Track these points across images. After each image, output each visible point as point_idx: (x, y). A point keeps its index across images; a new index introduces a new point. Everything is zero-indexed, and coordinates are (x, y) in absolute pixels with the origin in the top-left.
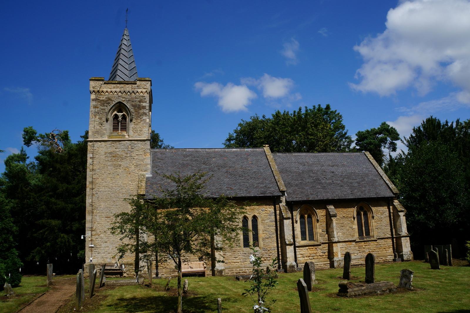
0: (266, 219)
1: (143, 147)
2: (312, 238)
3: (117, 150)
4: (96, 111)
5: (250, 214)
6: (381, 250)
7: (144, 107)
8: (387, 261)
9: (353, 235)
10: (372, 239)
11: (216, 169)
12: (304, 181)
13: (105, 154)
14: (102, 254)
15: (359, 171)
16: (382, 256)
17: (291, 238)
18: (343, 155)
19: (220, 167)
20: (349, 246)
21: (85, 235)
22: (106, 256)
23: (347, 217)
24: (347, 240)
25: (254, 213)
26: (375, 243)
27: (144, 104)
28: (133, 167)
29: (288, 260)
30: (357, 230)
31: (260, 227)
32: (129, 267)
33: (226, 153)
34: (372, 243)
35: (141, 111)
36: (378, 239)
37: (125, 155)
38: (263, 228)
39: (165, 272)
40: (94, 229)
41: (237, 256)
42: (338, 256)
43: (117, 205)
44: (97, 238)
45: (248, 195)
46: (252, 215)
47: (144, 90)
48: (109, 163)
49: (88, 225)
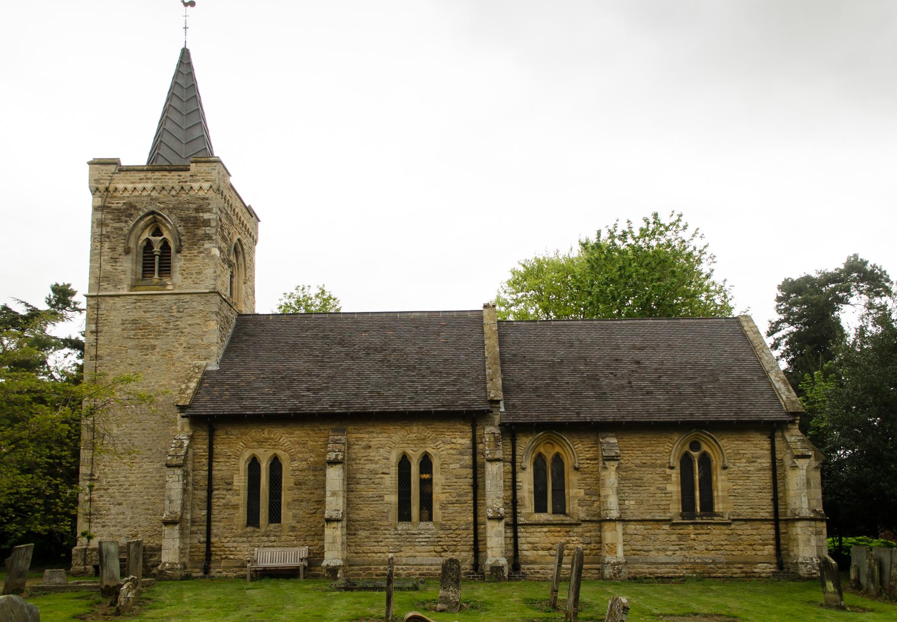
1: (201, 307)
2: (560, 507)
3: (148, 315)
4: (104, 233)
6: (740, 547)
7: (207, 223)
8: (757, 575)
9: (666, 507)
10: (717, 519)
11: (362, 354)
12: (557, 380)
13: (123, 324)
14: (112, 528)
15: (708, 361)
16: (740, 563)
17: (501, 505)
18: (679, 323)
19: (369, 350)
20: (650, 531)
22: (119, 533)
23: (653, 466)
24: (648, 517)
27: (206, 216)
28: (181, 349)
29: (489, 552)
33: (396, 321)
34: (716, 531)
35: (200, 232)
36: (734, 520)
37: (164, 325)
38: (443, 481)
39: (224, 567)
40: (95, 478)
42: (616, 553)
43: (144, 429)
44: (102, 496)
45: (413, 408)
46: (421, 451)
47: (206, 185)
48: (131, 343)
49: (84, 470)
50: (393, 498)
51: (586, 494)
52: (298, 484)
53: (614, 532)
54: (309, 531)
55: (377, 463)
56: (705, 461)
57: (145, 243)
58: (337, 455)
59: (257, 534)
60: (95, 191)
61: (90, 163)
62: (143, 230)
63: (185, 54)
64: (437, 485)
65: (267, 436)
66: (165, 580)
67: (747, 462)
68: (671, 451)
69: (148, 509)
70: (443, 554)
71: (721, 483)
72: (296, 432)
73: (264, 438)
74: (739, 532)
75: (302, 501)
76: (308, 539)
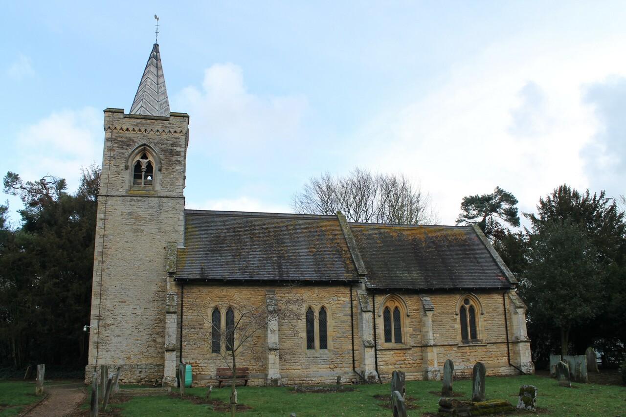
2: (399, 339)
6: (491, 359)
7: (178, 153)
9: (455, 337)
20: (448, 352)
23: (448, 313)
24: (446, 343)
27: (178, 149)
30: (459, 331)
31: (330, 322)
34: (480, 349)
35: (174, 158)
42: (433, 365)
43: (135, 286)
49: (94, 312)
51: (414, 331)
53: (432, 353)
56: (472, 310)
57: (136, 164)
59: (219, 358)
61: (105, 111)
62: (137, 155)
63: (156, 46)
64: (96, 260)
65: (225, 294)
66: (244, 408)
67: (493, 310)
68: (456, 305)
69: (137, 340)
70: (334, 369)
71: (481, 323)
72: (244, 292)
73: (224, 295)
74: (491, 350)
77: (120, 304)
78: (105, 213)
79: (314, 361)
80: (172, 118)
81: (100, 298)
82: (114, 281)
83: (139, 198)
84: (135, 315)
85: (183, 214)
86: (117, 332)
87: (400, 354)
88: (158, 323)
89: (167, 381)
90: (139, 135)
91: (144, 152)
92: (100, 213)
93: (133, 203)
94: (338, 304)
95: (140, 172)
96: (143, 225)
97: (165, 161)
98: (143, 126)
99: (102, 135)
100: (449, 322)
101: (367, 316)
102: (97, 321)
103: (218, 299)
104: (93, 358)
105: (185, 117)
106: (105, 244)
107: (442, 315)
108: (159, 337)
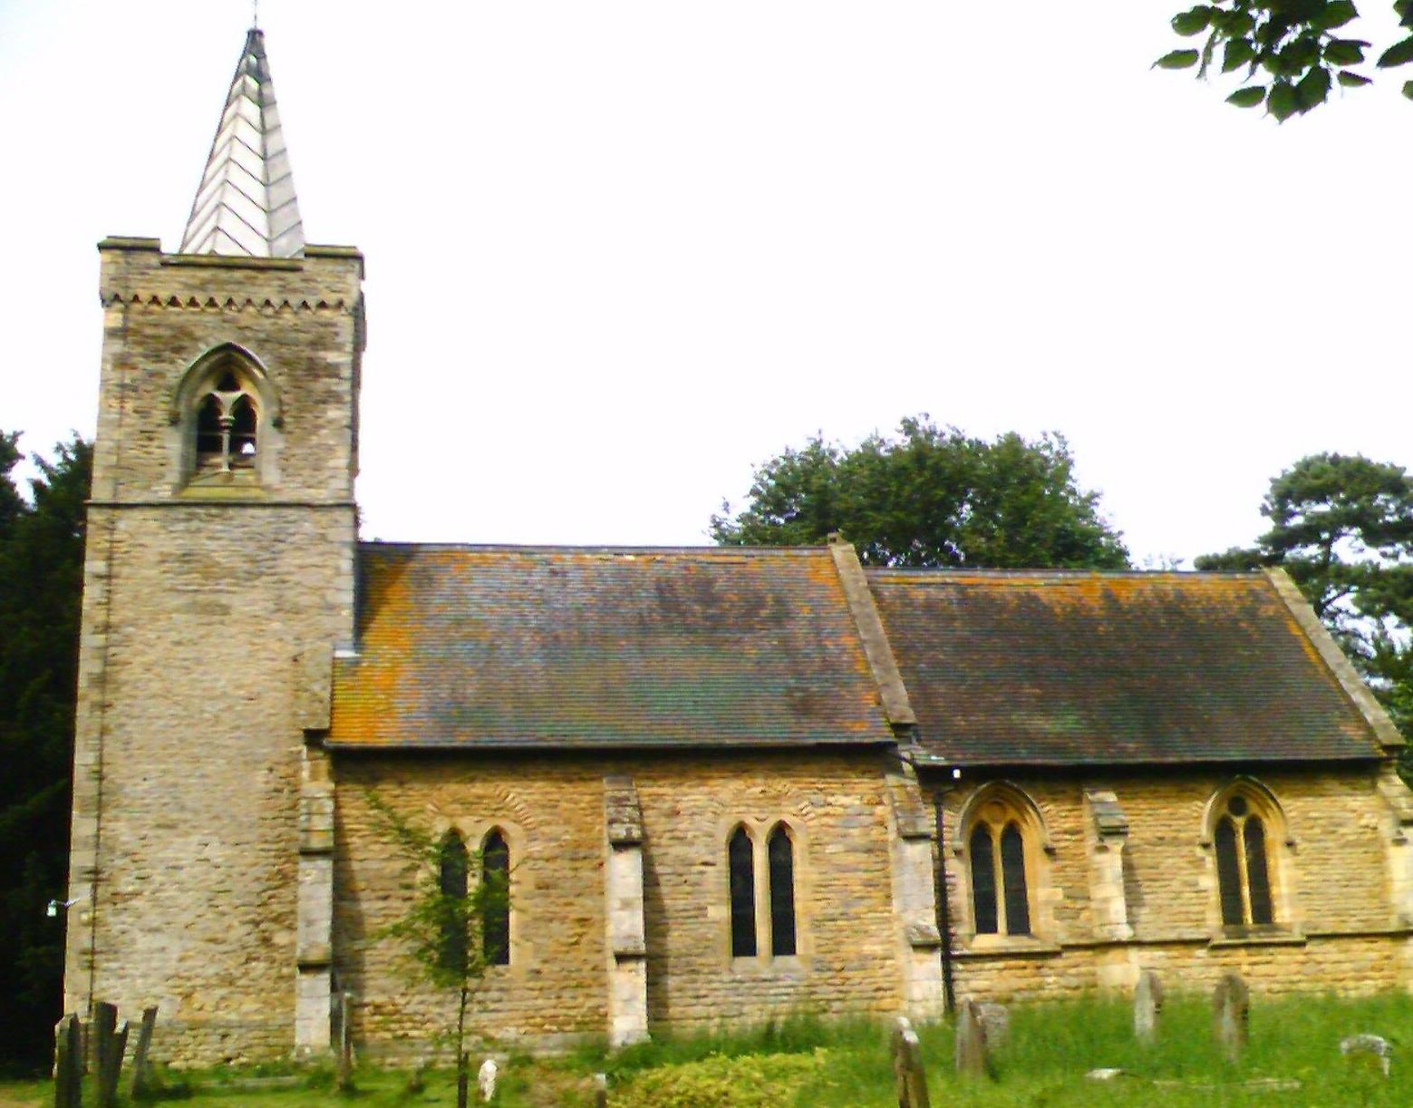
0: (826, 839)
2: (1019, 924)
4: (127, 381)
5: (763, 816)
7: (333, 371)
9: (1200, 917)
20: (1179, 962)
21: (66, 901)
23: (1175, 842)
24: (1172, 936)
25: (781, 812)
26: (1298, 955)
27: (332, 357)
30: (1214, 897)
31: (802, 872)
32: (250, 1035)
34: (1282, 956)
36: (1311, 937)
41: (703, 992)
49: (80, 859)
50: (721, 912)
52: (544, 886)
53: (1126, 965)
54: (565, 978)
55: (691, 844)
58: (629, 830)
60: (109, 300)
63: (255, 36)
67: (1324, 833)
74: (1319, 958)
75: (551, 920)
76: (566, 994)
77: (160, 832)
78: (110, 558)
79: (755, 992)
80: (309, 265)
81: (99, 817)
82: (138, 763)
83: (214, 511)
84: (205, 866)
85: (349, 553)
86: (154, 919)
87: (1025, 968)
88: (276, 888)
89: (302, 1060)
90: (210, 317)
91: (228, 366)
92: (94, 559)
93: (195, 524)
94: (827, 815)
95: (216, 433)
96: (229, 592)
97: (291, 396)
98: (223, 290)
99: (98, 319)
100: (1181, 868)
101: (920, 853)
102: (89, 886)
103: (458, 806)
104: (77, 997)
105: (352, 258)
106: (113, 650)
107: (1158, 848)
108: (280, 930)
